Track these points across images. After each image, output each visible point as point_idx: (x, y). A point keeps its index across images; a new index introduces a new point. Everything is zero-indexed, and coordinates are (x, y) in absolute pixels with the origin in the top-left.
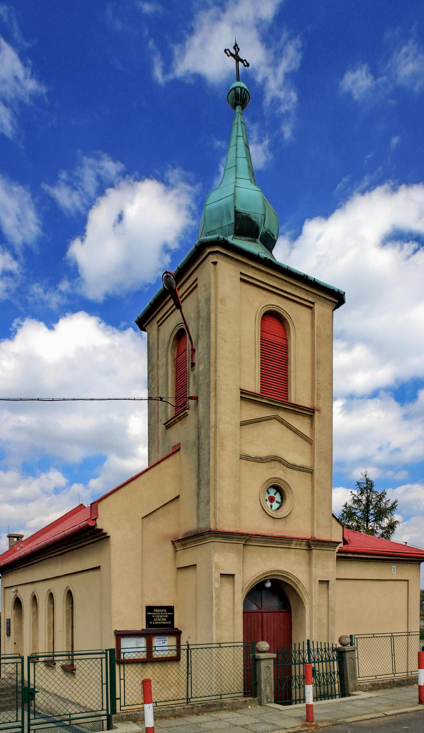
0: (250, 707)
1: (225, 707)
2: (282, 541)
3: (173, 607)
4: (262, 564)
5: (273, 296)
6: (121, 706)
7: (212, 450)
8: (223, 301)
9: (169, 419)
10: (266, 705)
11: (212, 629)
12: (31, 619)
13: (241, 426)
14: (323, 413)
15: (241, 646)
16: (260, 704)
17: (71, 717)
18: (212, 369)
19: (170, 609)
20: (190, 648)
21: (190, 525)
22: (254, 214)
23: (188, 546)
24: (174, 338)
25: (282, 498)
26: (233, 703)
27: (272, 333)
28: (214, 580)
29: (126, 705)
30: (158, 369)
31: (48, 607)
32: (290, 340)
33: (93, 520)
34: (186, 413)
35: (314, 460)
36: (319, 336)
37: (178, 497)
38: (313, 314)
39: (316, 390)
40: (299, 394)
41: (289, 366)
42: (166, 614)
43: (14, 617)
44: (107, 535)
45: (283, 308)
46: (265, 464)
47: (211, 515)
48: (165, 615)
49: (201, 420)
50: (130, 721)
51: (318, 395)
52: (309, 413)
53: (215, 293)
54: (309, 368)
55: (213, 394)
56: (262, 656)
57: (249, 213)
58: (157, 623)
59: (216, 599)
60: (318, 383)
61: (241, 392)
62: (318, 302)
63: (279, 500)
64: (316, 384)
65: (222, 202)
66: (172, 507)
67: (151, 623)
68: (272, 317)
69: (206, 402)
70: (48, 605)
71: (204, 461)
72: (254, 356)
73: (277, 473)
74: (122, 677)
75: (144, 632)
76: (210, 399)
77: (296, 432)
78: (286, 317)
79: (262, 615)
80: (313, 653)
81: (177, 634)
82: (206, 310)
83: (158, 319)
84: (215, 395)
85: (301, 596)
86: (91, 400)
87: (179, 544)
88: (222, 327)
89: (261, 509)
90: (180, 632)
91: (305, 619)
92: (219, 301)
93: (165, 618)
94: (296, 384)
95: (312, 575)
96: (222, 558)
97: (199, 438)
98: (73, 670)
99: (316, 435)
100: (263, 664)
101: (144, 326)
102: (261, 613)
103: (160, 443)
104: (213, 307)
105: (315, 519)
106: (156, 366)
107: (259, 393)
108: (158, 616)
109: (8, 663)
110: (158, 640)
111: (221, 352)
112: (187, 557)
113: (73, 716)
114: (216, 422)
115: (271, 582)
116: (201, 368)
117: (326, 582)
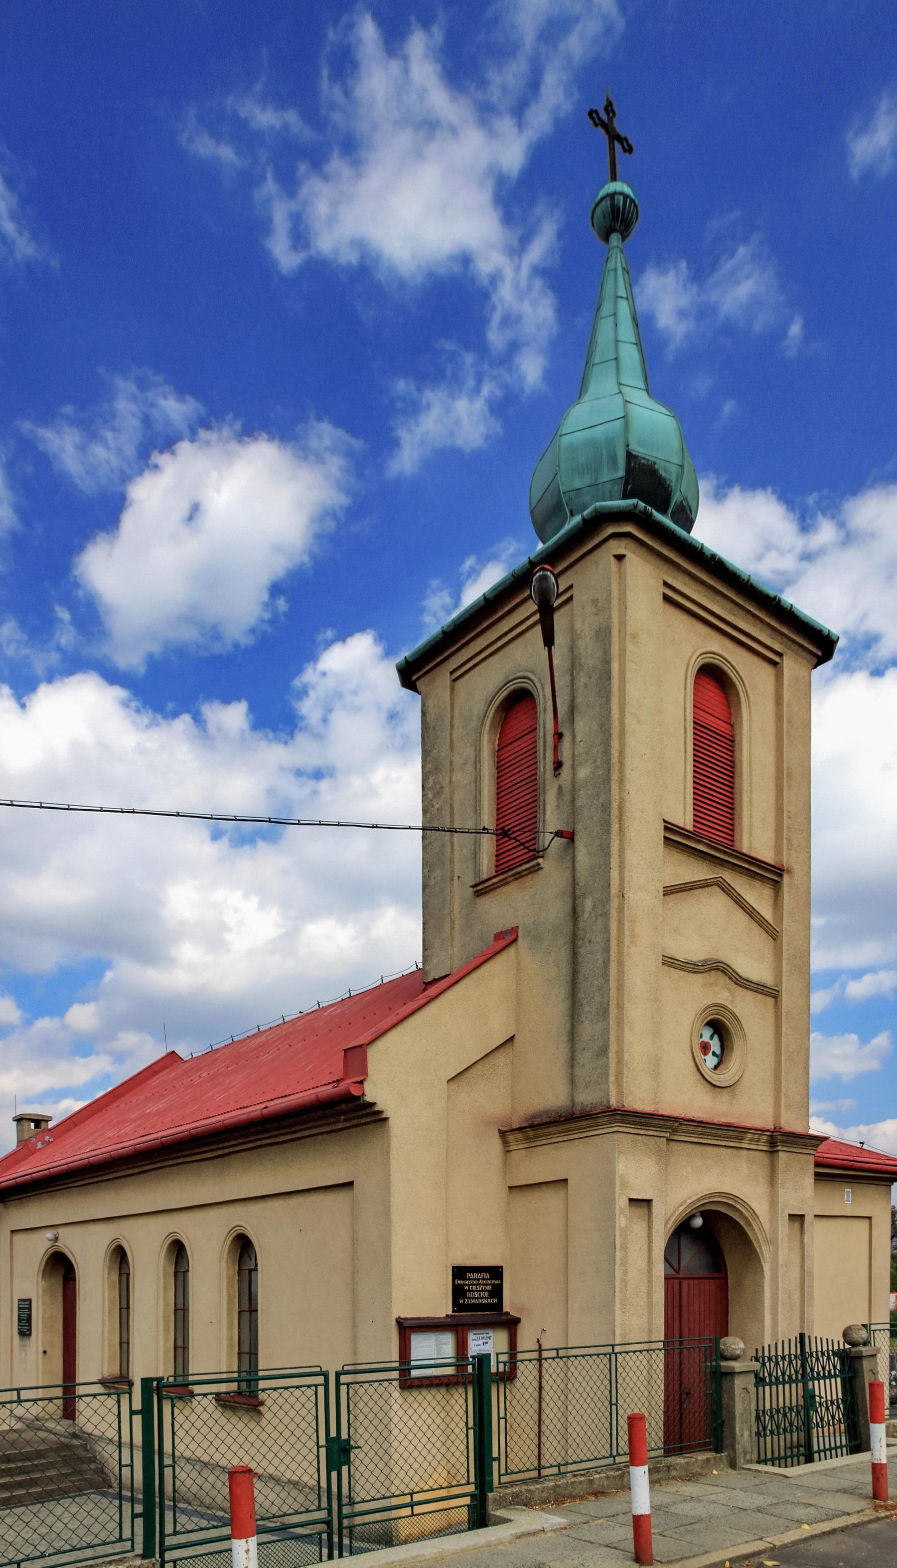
0: (715, 1472)
1: (674, 1473)
2: (730, 1133)
3: (502, 1267)
4: (692, 1181)
5: (713, 634)
6: (500, 1475)
7: (613, 942)
8: (634, 636)
9: (485, 877)
10: (745, 1466)
11: (613, 1313)
12: (106, 1297)
13: (664, 895)
14: (796, 877)
15: (660, 1350)
16: (733, 1465)
17: (414, 1500)
18: (615, 776)
19: (496, 1272)
20: (616, 1351)
21: (552, 1095)
22: (663, 463)
23: (545, 1142)
24: (498, 707)
25: (722, 1047)
26: (687, 1463)
27: (706, 709)
28: (617, 1212)
29: (509, 1471)
30: (452, 770)
31: (164, 1270)
32: (741, 727)
33: (357, 1082)
34: (539, 864)
35: (781, 971)
36: (790, 722)
37: (512, 1038)
38: (779, 677)
39: (785, 831)
40: (756, 838)
41: (737, 780)
42: (489, 1282)
43: (43, 1295)
44: (384, 1116)
45: (730, 660)
46: (699, 977)
47: (612, 1079)
48: (487, 1285)
49: (582, 881)
50: (518, 1504)
51: (788, 840)
52: (772, 875)
53: (620, 618)
54: (771, 784)
55: (615, 827)
56: (737, 1366)
57: (653, 459)
58: (473, 1301)
59: (620, 1250)
60: (789, 817)
61: (666, 829)
62: (789, 652)
63: (718, 1052)
64: (785, 818)
65: (598, 432)
66: (501, 1060)
67: (461, 1301)
68: (713, 677)
69: (597, 843)
70: (164, 1267)
71: (587, 967)
72: (682, 754)
73: (720, 996)
74: (502, 1415)
75: (449, 1320)
76: (609, 838)
77: (752, 913)
78: (735, 680)
79: (680, 1284)
80: (809, 1360)
81: (511, 1324)
82: (600, 654)
83: (455, 667)
84: (621, 831)
85: (756, 1245)
86: (373, 827)
87: (520, 1136)
88: (633, 692)
89: (695, 1069)
90: (517, 1321)
91: (763, 1292)
92: (628, 637)
93: (486, 1290)
94: (751, 817)
95: (778, 1203)
96: (635, 1167)
97: (575, 914)
98: (257, 1406)
99: (785, 922)
100: (738, 1382)
101: (414, 678)
102: (677, 1281)
103: (457, 926)
104: (615, 649)
105: (783, 1090)
106: (447, 765)
107: (691, 828)
108: (474, 1288)
109: (266, 1389)
110: (475, 1337)
111: (633, 743)
112: (542, 1162)
113: (416, 1498)
114: (621, 885)
115: (701, 1216)
116: (583, 773)
117: (798, 1218)
